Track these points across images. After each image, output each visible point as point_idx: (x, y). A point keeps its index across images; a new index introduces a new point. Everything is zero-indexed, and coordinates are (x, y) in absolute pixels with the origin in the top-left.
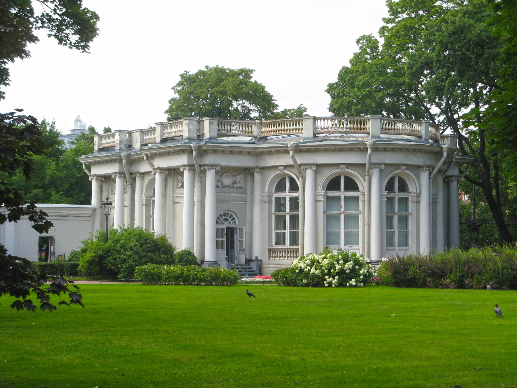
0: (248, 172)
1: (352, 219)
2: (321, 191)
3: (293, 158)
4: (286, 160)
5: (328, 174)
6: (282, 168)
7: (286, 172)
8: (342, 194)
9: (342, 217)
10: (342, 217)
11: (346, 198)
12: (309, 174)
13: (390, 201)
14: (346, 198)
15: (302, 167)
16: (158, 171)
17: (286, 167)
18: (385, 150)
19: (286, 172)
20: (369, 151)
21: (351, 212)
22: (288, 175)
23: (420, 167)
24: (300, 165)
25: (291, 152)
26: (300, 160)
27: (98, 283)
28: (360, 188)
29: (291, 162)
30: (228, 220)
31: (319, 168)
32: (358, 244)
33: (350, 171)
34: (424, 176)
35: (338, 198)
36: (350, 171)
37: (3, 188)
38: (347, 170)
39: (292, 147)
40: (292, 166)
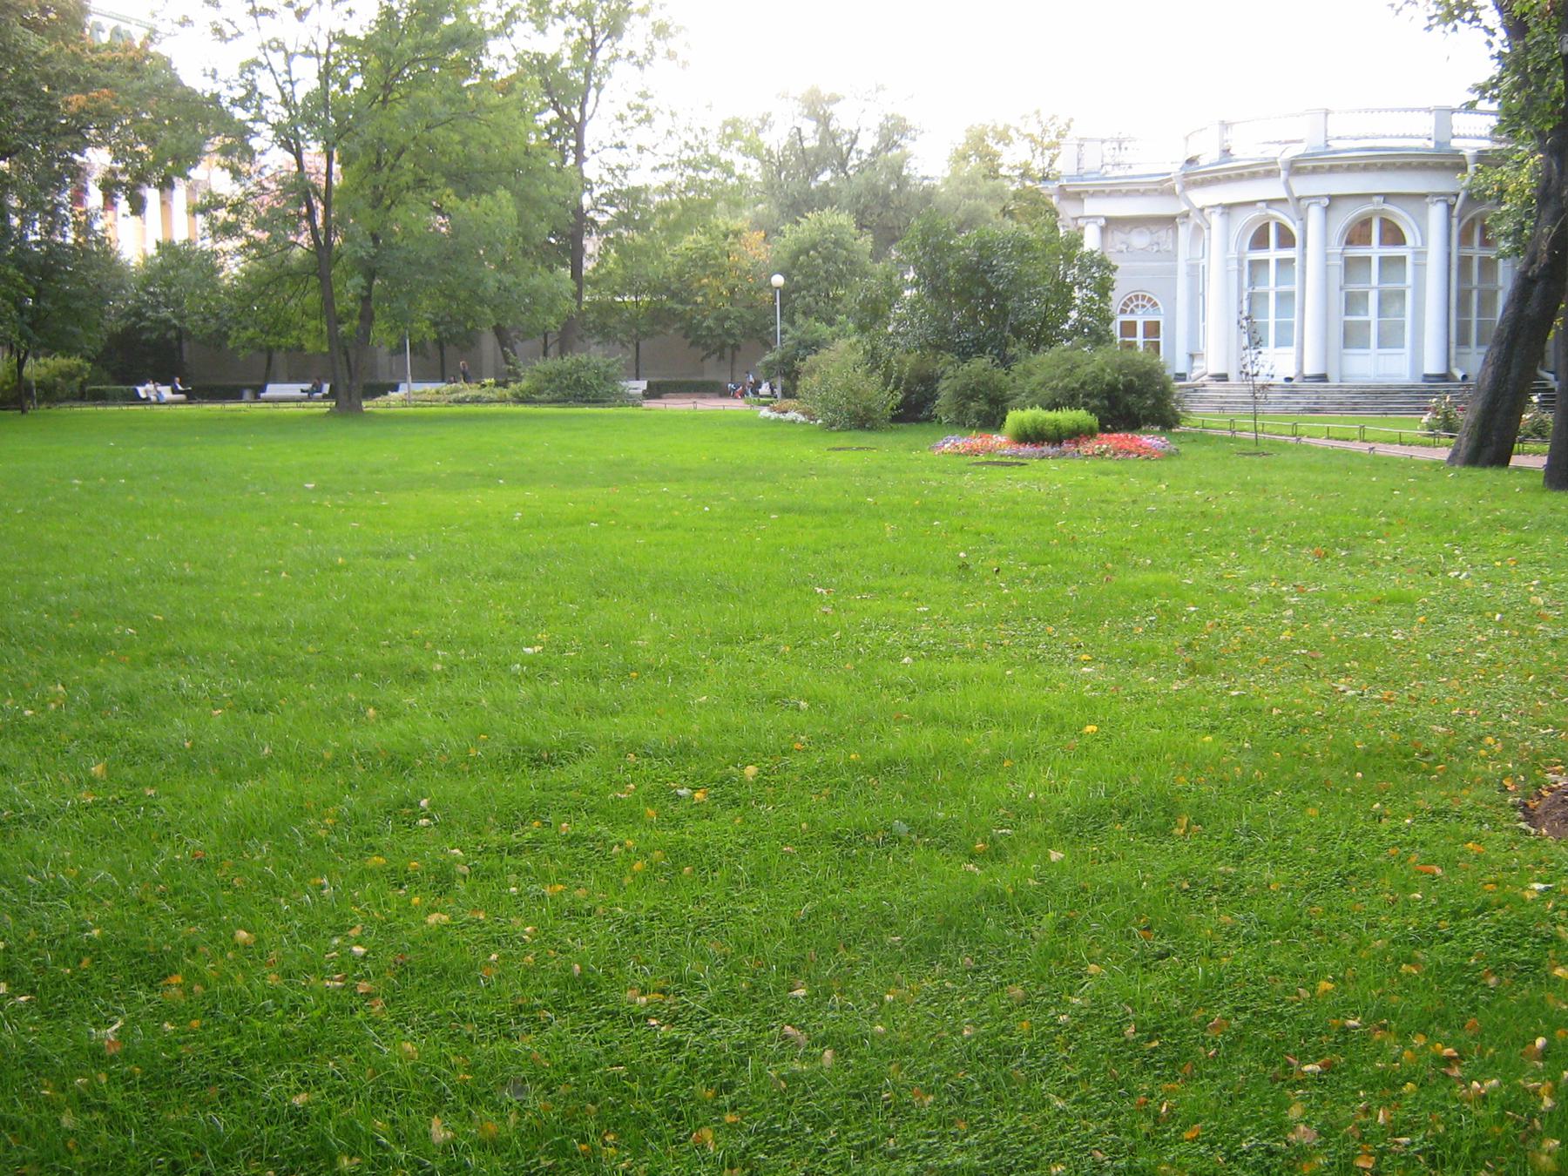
0: (1170, 221)
1: (1285, 299)
2: (1336, 248)
3: (1287, 184)
4: (1273, 189)
5: (1346, 216)
6: (1264, 205)
7: (1272, 212)
8: (1273, 254)
9: (1373, 297)
10: (1373, 297)
11: (1382, 260)
12: (1315, 215)
13: (1354, 267)
14: (1382, 260)
15: (1302, 202)
16: (1219, 210)
17: (1270, 202)
18: (1315, 170)
19: (1272, 212)
20: (1283, 174)
21: (1258, 289)
22: (1274, 218)
23: (1425, 196)
24: (1299, 199)
25: (1283, 174)
26: (1302, 186)
27: (217, 407)
28: (1410, 241)
29: (1283, 195)
30: (1143, 306)
31: (1228, 208)
32: (1402, 346)
33: (1276, 213)
34: (1436, 213)
35: (1266, 262)
36: (1276, 213)
37: (3, 310)
38: (1387, 207)
39: (1284, 162)
40: (1284, 201)
